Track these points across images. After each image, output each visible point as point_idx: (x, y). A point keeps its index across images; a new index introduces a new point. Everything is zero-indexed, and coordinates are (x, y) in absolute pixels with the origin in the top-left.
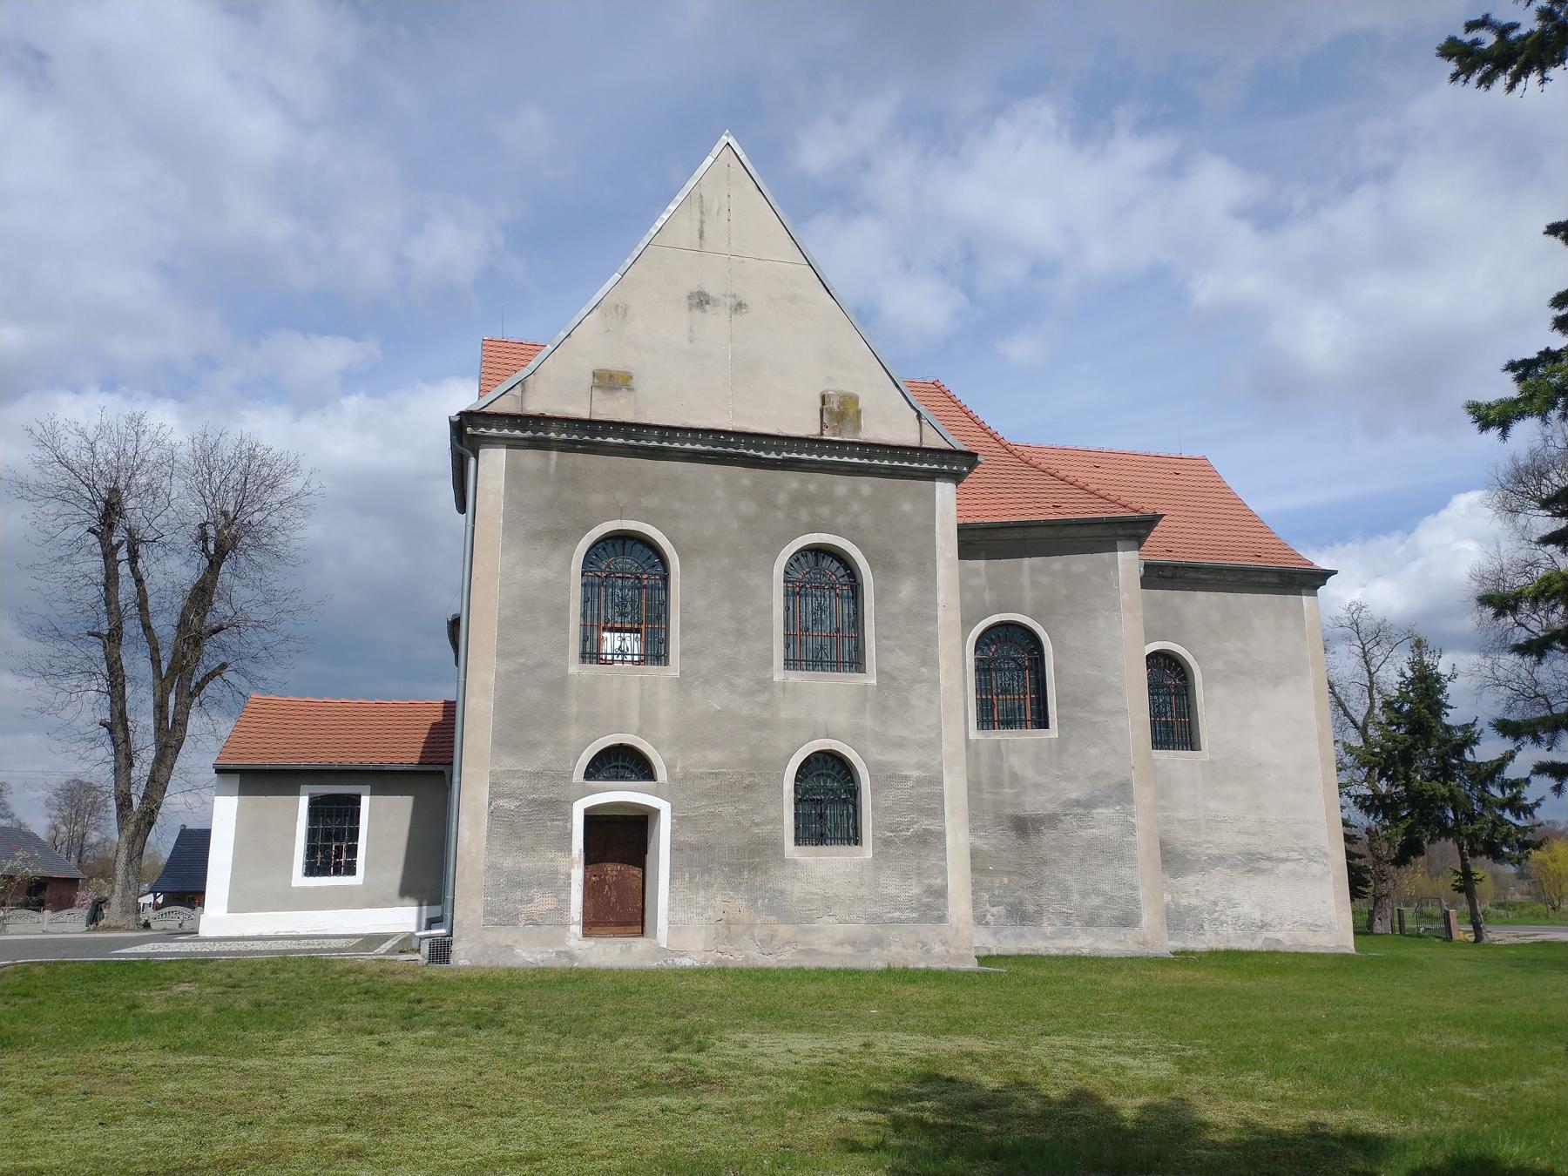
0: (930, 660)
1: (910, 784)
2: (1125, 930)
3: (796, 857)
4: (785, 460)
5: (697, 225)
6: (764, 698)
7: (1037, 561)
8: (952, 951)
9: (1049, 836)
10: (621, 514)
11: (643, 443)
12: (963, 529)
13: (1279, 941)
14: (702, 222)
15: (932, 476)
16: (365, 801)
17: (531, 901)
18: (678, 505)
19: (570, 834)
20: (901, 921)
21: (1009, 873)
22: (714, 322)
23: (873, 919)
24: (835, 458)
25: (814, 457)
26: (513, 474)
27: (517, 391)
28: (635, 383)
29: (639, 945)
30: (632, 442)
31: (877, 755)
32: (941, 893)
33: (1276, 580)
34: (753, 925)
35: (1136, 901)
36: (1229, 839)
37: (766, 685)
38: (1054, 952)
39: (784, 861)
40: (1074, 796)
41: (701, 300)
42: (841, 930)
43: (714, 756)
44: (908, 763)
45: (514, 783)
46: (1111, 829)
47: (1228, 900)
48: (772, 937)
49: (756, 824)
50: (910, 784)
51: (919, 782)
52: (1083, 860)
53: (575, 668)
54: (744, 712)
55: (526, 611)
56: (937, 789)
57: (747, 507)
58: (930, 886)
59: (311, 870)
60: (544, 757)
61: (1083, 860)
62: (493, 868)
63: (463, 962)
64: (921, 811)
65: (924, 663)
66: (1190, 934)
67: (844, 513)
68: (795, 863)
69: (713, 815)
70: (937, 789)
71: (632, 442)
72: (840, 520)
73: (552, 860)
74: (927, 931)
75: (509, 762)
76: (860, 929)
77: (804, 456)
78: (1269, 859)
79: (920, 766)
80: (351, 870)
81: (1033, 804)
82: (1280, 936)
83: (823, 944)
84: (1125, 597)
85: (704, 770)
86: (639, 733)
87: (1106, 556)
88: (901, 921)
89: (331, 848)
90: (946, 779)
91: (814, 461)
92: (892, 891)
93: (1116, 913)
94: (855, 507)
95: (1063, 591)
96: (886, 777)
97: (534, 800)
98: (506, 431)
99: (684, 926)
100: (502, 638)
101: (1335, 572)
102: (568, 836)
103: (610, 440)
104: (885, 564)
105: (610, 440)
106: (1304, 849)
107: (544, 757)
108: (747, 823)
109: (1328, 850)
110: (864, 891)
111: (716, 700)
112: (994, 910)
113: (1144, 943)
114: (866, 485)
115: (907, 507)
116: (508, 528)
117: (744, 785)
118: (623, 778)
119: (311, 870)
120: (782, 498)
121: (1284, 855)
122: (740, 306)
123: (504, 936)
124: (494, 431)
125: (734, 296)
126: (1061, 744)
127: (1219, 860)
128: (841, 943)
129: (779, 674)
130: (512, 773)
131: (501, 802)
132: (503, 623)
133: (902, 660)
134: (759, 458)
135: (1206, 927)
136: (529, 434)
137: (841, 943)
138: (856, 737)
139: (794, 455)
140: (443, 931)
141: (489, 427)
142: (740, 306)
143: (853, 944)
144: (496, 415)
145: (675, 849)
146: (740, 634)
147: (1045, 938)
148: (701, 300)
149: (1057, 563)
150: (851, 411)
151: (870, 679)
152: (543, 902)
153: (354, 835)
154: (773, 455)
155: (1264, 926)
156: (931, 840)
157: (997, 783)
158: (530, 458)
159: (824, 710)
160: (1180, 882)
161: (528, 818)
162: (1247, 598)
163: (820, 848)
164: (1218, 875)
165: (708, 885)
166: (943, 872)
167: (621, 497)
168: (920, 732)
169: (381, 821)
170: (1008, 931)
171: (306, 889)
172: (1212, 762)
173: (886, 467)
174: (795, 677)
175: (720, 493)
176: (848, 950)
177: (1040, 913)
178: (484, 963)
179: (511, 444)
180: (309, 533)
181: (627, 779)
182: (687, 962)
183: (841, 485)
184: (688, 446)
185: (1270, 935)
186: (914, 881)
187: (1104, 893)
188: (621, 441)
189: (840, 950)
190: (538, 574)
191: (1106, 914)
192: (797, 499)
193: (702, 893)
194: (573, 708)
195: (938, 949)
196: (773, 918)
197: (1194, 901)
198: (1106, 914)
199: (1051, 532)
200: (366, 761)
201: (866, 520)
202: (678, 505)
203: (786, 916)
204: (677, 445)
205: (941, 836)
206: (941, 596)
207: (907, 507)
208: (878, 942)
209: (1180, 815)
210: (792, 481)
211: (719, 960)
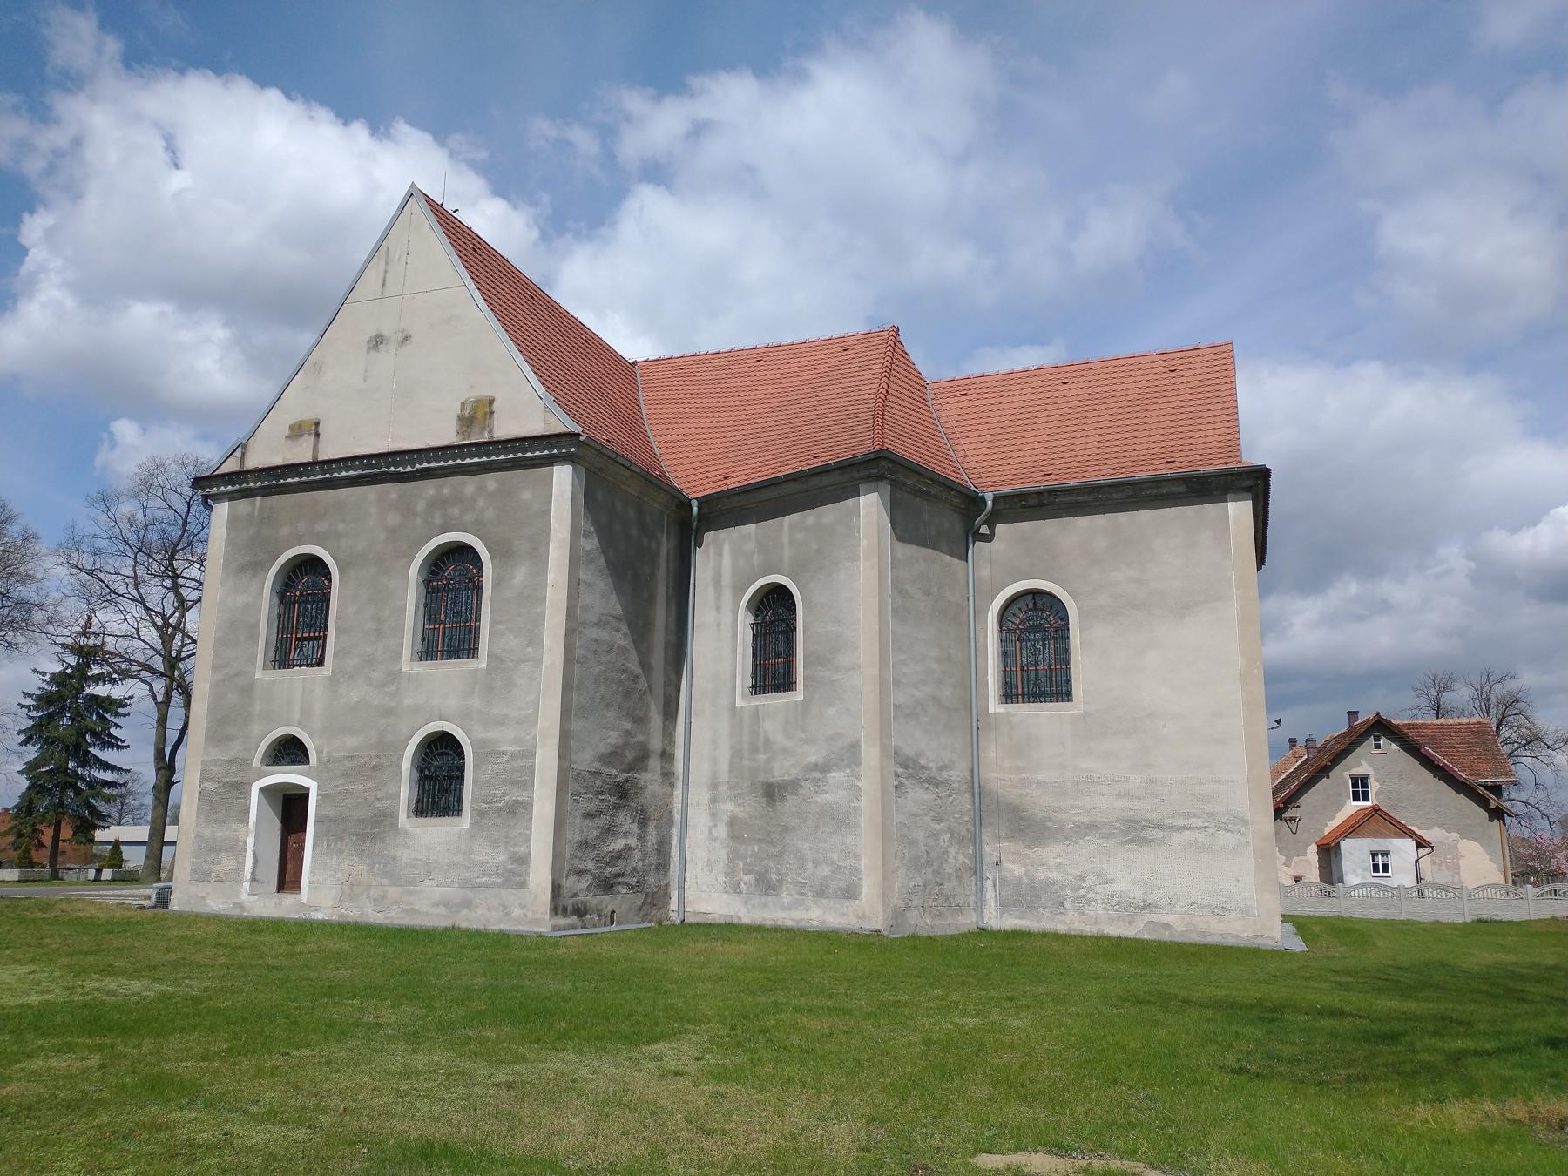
0: (535, 641)
2: (847, 903)
3: (408, 827)
4: (420, 471)
5: (381, 275)
6: (393, 688)
7: (795, 517)
8: (529, 914)
9: (791, 802)
13: (1167, 926)
15: (549, 461)
18: (341, 527)
19: (248, 810)
21: (760, 841)
22: (386, 357)
23: (465, 883)
26: (233, 520)
27: (238, 453)
31: (480, 733)
32: (523, 860)
33: (1182, 488)
34: (369, 886)
36: (1105, 804)
37: (395, 676)
38: (790, 923)
40: (813, 759)
41: (377, 341)
42: (437, 892)
43: (351, 741)
44: (506, 739)
46: (842, 793)
47: (1099, 875)
48: (383, 897)
51: (514, 756)
52: (817, 827)
55: (235, 629)
56: (528, 762)
57: (393, 519)
58: (514, 853)
60: (235, 749)
61: (817, 827)
62: (198, 835)
63: (176, 908)
65: (530, 643)
66: (1047, 913)
67: (465, 512)
68: (406, 832)
69: (348, 792)
70: (528, 762)
74: (509, 895)
75: (214, 753)
76: (453, 892)
77: (434, 464)
81: (782, 770)
86: (300, 725)
88: (487, 886)
92: (482, 858)
93: (842, 884)
94: (481, 503)
95: (814, 546)
96: (488, 753)
99: (323, 893)
104: (503, 553)
106: (1212, 814)
107: (235, 749)
108: (371, 799)
109: (1248, 816)
110: (459, 858)
111: (355, 693)
112: (746, 878)
113: (863, 917)
114: (491, 481)
116: (225, 567)
117: (374, 767)
120: (421, 506)
121: (1181, 822)
123: (200, 889)
126: (806, 702)
127: (1092, 827)
128: (436, 905)
129: (408, 665)
130: (214, 762)
133: (512, 642)
135: (1068, 905)
137: (436, 905)
138: (464, 718)
142: (406, 338)
143: (447, 905)
145: (318, 821)
146: (379, 633)
147: (784, 909)
149: (810, 517)
151: (481, 663)
152: (227, 864)
154: (409, 469)
155: (1146, 906)
156: (519, 811)
157: (754, 750)
158: (243, 505)
159: (441, 695)
160: (1038, 852)
161: (225, 796)
162: (1145, 516)
163: (445, 819)
164: (1087, 846)
165: (340, 851)
166: (528, 840)
167: (302, 526)
170: (755, 901)
172: (1085, 715)
176: (442, 910)
177: (780, 882)
179: (231, 497)
182: (319, 916)
183: (469, 484)
185: (1154, 917)
186: (501, 849)
187: (833, 863)
189: (435, 911)
190: (241, 599)
191: (834, 885)
192: (433, 504)
194: (257, 707)
195: (517, 912)
196: (385, 881)
197: (1053, 875)
198: (834, 885)
199: (793, 487)
201: (490, 514)
205: (528, 806)
206: (551, 577)
207: (526, 495)
208: (467, 904)
209: (1041, 777)
210: (429, 488)
211: (342, 915)
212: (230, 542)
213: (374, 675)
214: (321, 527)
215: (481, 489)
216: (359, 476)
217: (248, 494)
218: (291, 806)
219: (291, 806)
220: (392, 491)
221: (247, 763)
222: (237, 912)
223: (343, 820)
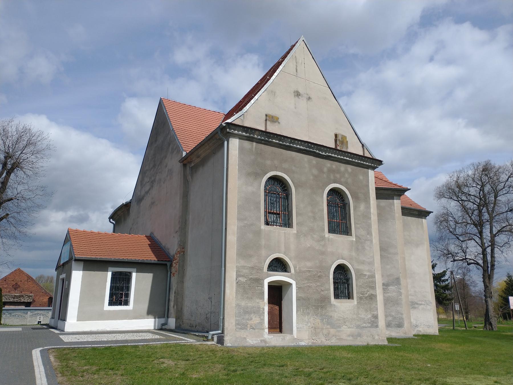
0: (370, 233)
1: (366, 277)
2: (399, 329)
5: (295, 67)
6: (322, 243)
10: (276, 169)
11: (284, 143)
12: (377, 189)
14: (297, 66)
15: (368, 167)
16: (134, 275)
17: (251, 319)
18: (294, 168)
19: (264, 292)
20: (366, 327)
22: (302, 103)
23: (358, 327)
24: (342, 157)
25: (336, 156)
26: (241, 149)
28: (280, 120)
29: (288, 337)
30: (281, 142)
32: (376, 317)
33: (417, 213)
34: (322, 329)
35: (403, 319)
37: (323, 238)
39: (331, 305)
42: (349, 331)
43: (309, 264)
44: (365, 269)
45: (244, 271)
46: (394, 294)
48: (329, 334)
49: (322, 291)
50: (366, 277)
53: (263, 227)
54: (317, 248)
57: (315, 172)
58: (373, 314)
59: (111, 303)
62: (238, 306)
63: (229, 345)
64: (370, 287)
65: (368, 234)
68: (334, 305)
69: (309, 286)
71: (281, 142)
72: (343, 180)
73: (258, 303)
74: (373, 330)
75: (242, 263)
77: (333, 155)
78: (417, 304)
79: (369, 271)
80: (126, 303)
82: (420, 329)
83: (344, 336)
84: (397, 215)
85: (305, 269)
86: (285, 254)
87: (391, 201)
88: (366, 327)
89: (119, 295)
90: (376, 276)
91: (336, 157)
92: (363, 316)
93: (397, 323)
96: (360, 274)
97: (251, 278)
98: (240, 132)
99: (301, 330)
100: (239, 213)
101: (432, 212)
102: (263, 293)
103: (274, 141)
104: (356, 197)
105: (274, 141)
110: (355, 316)
113: (405, 333)
114: (350, 168)
115: (361, 177)
116: (240, 170)
117: (318, 276)
118: (276, 271)
119: (111, 303)
120: (325, 170)
121: (420, 303)
122: (309, 98)
123: (243, 334)
124: (236, 132)
125: (307, 94)
128: (349, 336)
129: (327, 235)
130: (244, 267)
131: (240, 279)
132: (239, 207)
133: (362, 232)
134: (319, 154)
136: (248, 135)
137: (349, 336)
138: (350, 259)
139: (330, 154)
140: (220, 332)
141: (235, 130)
143: (353, 336)
144: (235, 125)
145: (298, 299)
148: (298, 94)
150: (345, 141)
151: (353, 238)
152: (255, 320)
153: (128, 288)
154: (324, 154)
155: (417, 326)
156: (372, 298)
158: (247, 144)
159: (340, 249)
165: (308, 314)
167: (276, 162)
168: (368, 259)
169: (140, 284)
171: (110, 311)
173: (356, 163)
174: (332, 236)
175: (307, 165)
178: (236, 345)
179: (241, 137)
180: (45, 163)
181: (278, 271)
182: (303, 344)
183: (343, 167)
184: (298, 146)
185: (418, 329)
188: (277, 141)
190: (250, 189)
191: (393, 323)
193: (307, 317)
194: (263, 242)
195: (377, 337)
196: (329, 326)
198: (393, 323)
200: (137, 259)
201: (350, 181)
202: (294, 168)
203: (333, 326)
204: (295, 146)
205: (375, 296)
206: (372, 210)
207: (361, 177)
208: (359, 335)
210: (328, 164)
211: (313, 343)
212: (241, 159)
213: (315, 236)
214: (285, 166)
215: (346, 170)
216: (304, 150)
217: (250, 139)
218: (277, 293)
219: (277, 293)
220: (315, 160)
221: (261, 269)
222: (263, 344)
223: (309, 299)
